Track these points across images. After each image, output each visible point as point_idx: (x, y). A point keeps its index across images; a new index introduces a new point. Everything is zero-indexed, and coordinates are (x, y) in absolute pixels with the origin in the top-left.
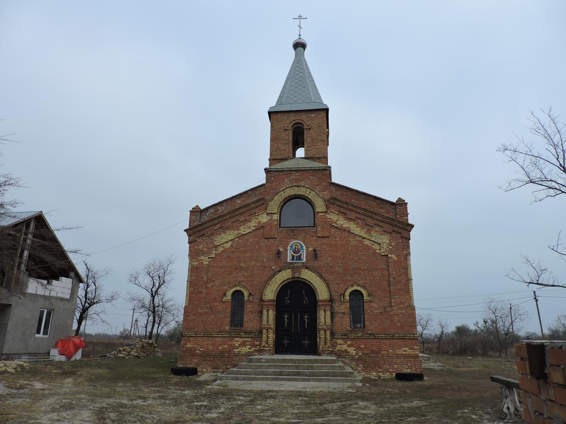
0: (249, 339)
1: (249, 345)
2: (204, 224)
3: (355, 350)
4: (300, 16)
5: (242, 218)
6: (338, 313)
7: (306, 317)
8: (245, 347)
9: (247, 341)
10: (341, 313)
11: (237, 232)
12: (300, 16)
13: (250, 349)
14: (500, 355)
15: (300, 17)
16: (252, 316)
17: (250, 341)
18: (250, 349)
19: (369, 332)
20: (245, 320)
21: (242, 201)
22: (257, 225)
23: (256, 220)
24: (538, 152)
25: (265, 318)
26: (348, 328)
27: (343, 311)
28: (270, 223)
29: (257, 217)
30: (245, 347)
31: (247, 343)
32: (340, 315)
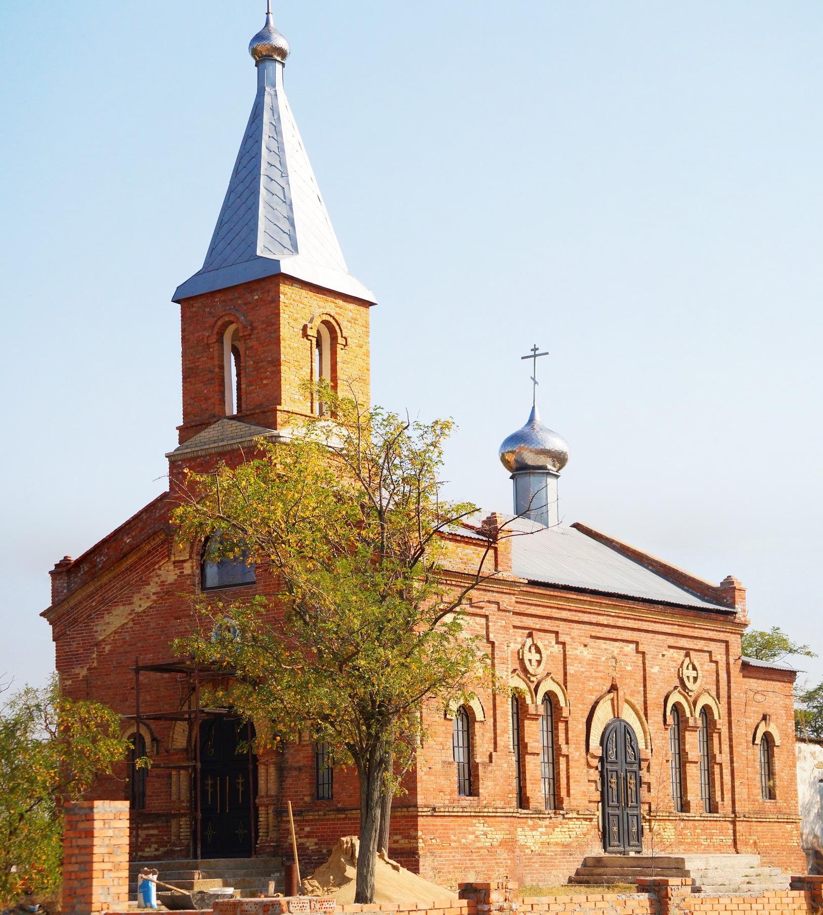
0: (155, 832)
1: (156, 843)
2: (82, 585)
3: (316, 844)
4: (535, 349)
5: (133, 577)
6: (290, 769)
7: (240, 781)
8: (150, 847)
9: (152, 835)
10: (296, 769)
11: (128, 609)
12: (535, 349)
13: (157, 850)
14: (646, 760)
15: (535, 353)
16: (157, 785)
17: (156, 835)
18: (157, 850)
19: (340, 805)
20: (148, 793)
21: (133, 537)
22: (159, 589)
23: (156, 579)
24: (441, 428)
25: (174, 788)
26: (307, 799)
27: (301, 764)
28: (179, 584)
29: (159, 572)
30: (150, 847)
31: (153, 840)
32: (295, 773)
